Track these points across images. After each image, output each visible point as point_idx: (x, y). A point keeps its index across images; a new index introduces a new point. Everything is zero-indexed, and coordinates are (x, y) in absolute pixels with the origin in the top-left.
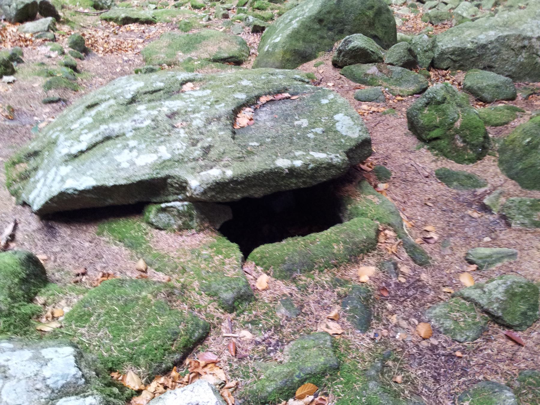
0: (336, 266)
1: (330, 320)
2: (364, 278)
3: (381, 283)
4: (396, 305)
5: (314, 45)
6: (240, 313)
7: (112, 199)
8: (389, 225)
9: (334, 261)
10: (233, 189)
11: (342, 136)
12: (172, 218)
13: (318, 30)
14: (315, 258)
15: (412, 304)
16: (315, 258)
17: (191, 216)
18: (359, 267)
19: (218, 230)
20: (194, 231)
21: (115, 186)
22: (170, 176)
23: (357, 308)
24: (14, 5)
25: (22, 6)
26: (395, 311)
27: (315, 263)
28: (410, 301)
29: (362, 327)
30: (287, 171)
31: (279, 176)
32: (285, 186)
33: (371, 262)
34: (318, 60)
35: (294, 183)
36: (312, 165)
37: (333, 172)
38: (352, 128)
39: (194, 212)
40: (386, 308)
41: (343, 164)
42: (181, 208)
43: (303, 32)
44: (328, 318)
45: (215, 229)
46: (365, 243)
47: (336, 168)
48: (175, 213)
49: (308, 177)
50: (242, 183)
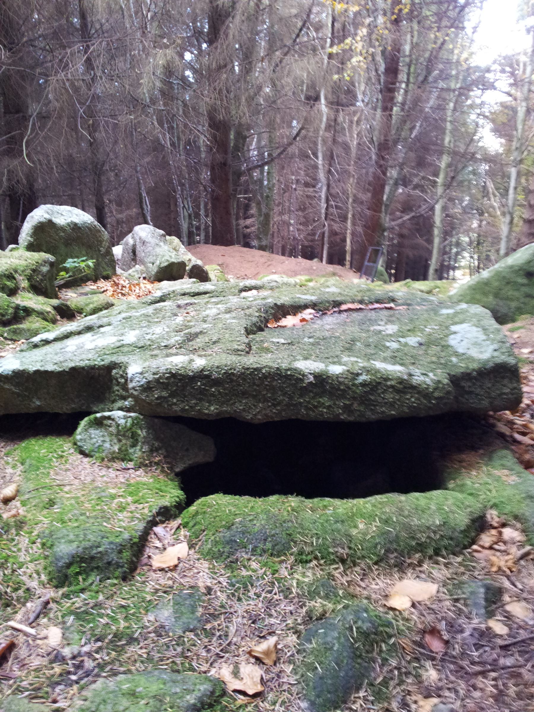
0: (343, 561)
1: (253, 660)
2: (400, 602)
3: (440, 621)
4: (452, 678)
5: (514, 304)
6: (74, 592)
7: (39, 399)
8: (516, 517)
9: (340, 550)
10: (202, 392)
11: (456, 354)
12: (107, 439)
13: (523, 285)
14: (299, 533)
15: (495, 686)
16: (299, 533)
17: (134, 436)
18: (401, 579)
19: (177, 474)
20: (131, 465)
21: (37, 372)
22: (116, 364)
23: (331, 649)
24: (158, 262)
25: (166, 264)
26: (440, 689)
27: (295, 542)
28: (495, 679)
29: (318, 696)
30: (311, 378)
31: (294, 385)
32: (307, 408)
33: (436, 573)
34: (517, 324)
35: (326, 408)
36: (363, 378)
37: (413, 400)
38: (479, 345)
39: (142, 433)
40: (418, 676)
41: (435, 389)
42: (122, 422)
43: (496, 284)
44: (250, 653)
45: (171, 469)
46: (435, 532)
47: (419, 392)
48: (113, 429)
49: (354, 398)
50: (217, 382)
